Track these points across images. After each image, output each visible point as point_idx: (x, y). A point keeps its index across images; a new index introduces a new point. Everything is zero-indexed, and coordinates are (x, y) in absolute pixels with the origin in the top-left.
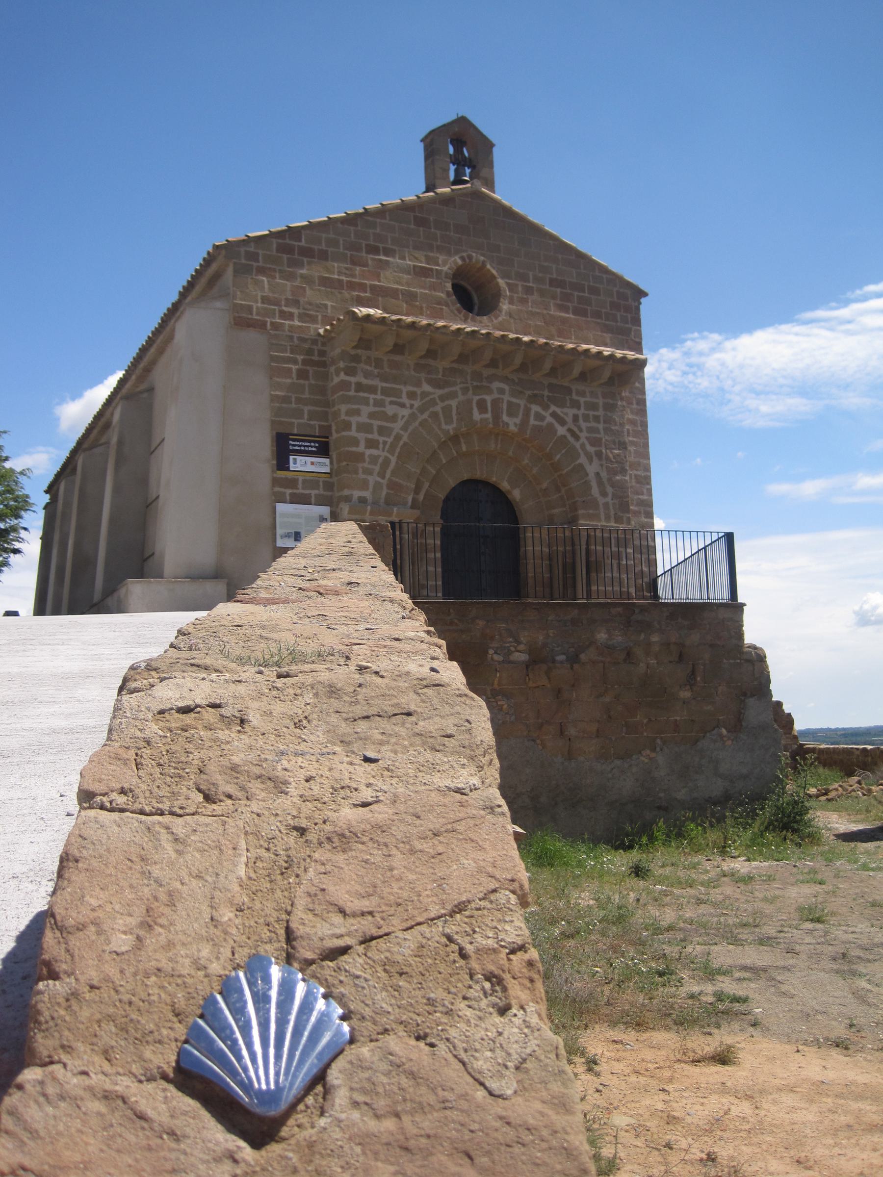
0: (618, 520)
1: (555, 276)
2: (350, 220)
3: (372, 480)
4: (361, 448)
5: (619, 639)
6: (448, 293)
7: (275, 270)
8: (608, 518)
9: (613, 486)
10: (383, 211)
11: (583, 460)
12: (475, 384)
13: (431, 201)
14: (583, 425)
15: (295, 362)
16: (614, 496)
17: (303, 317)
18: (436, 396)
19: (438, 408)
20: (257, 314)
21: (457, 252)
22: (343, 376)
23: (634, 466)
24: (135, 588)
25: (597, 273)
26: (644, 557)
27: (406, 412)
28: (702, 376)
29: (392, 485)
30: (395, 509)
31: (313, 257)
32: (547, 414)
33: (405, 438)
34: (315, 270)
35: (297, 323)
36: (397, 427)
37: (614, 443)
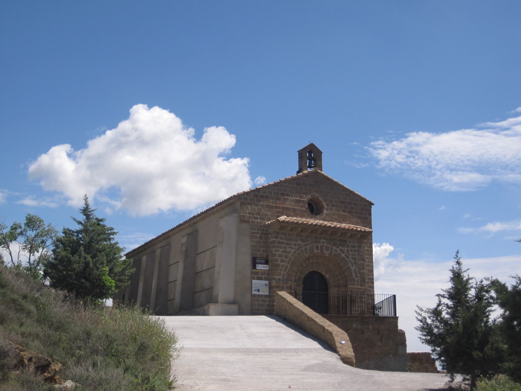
0: (361, 285)
3: (282, 273)
4: (279, 263)
6: (307, 209)
10: (286, 181)
11: (350, 265)
13: (302, 176)
14: (350, 253)
15: (258, 233)
17: (261, 219)
19: (303, 249)
22: (274, 239)
23: (367, 266)
24: (212, 307)
27: (293, 250)
28: (419, 159)
32: (338, 250)
34: (265, 203)
35: (259, 221)
36: (290, 255)
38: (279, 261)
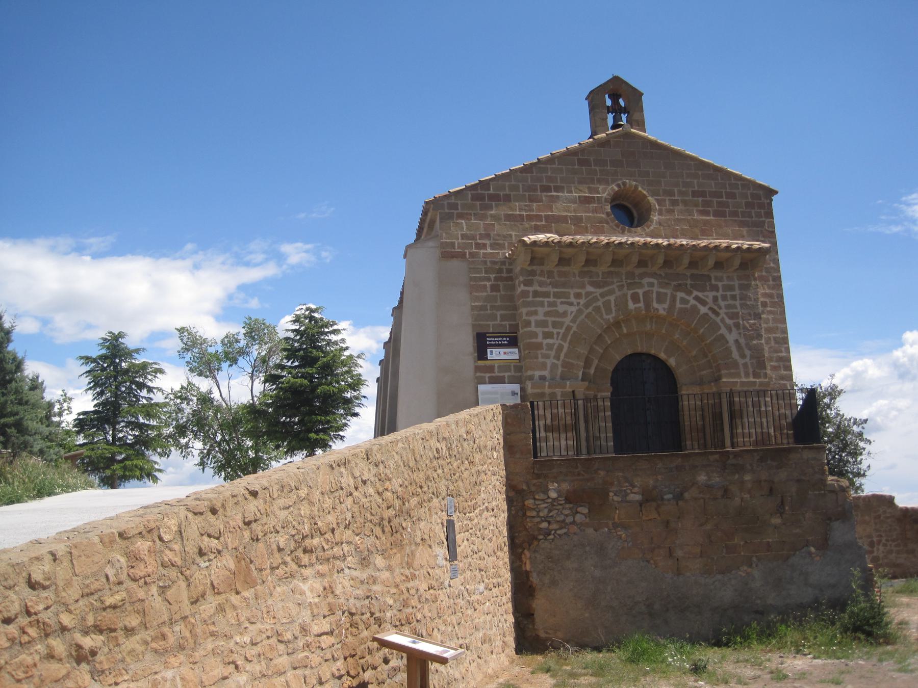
0: (756, 375)
1: (696, 188)
2: (527, 169)
3: (549, 362)
4: (540, 339)
5: (716, 479)
6: (608, 214)
7: (470, 214)
8: (747, 375)
9: (750, 349)
10: (553, 159)
12: (629, 281)
14: (722, 303)
15: (489, 279)
16: (752, 357)
18: (598, 294)
19: (600, 303)
20: (459, 248)
21: (613, 181)
22: (522, 287)
25: (733, 182)
26: (787, 402)
27: (574, 309)
29: (565, 365)
30: (568, 383)
31: (500, 200)
33: (574, 329)
34: (501, 210)
35: (489, 251)
36: (567, 321)
37: (750, 315)
38: (540, 336)
